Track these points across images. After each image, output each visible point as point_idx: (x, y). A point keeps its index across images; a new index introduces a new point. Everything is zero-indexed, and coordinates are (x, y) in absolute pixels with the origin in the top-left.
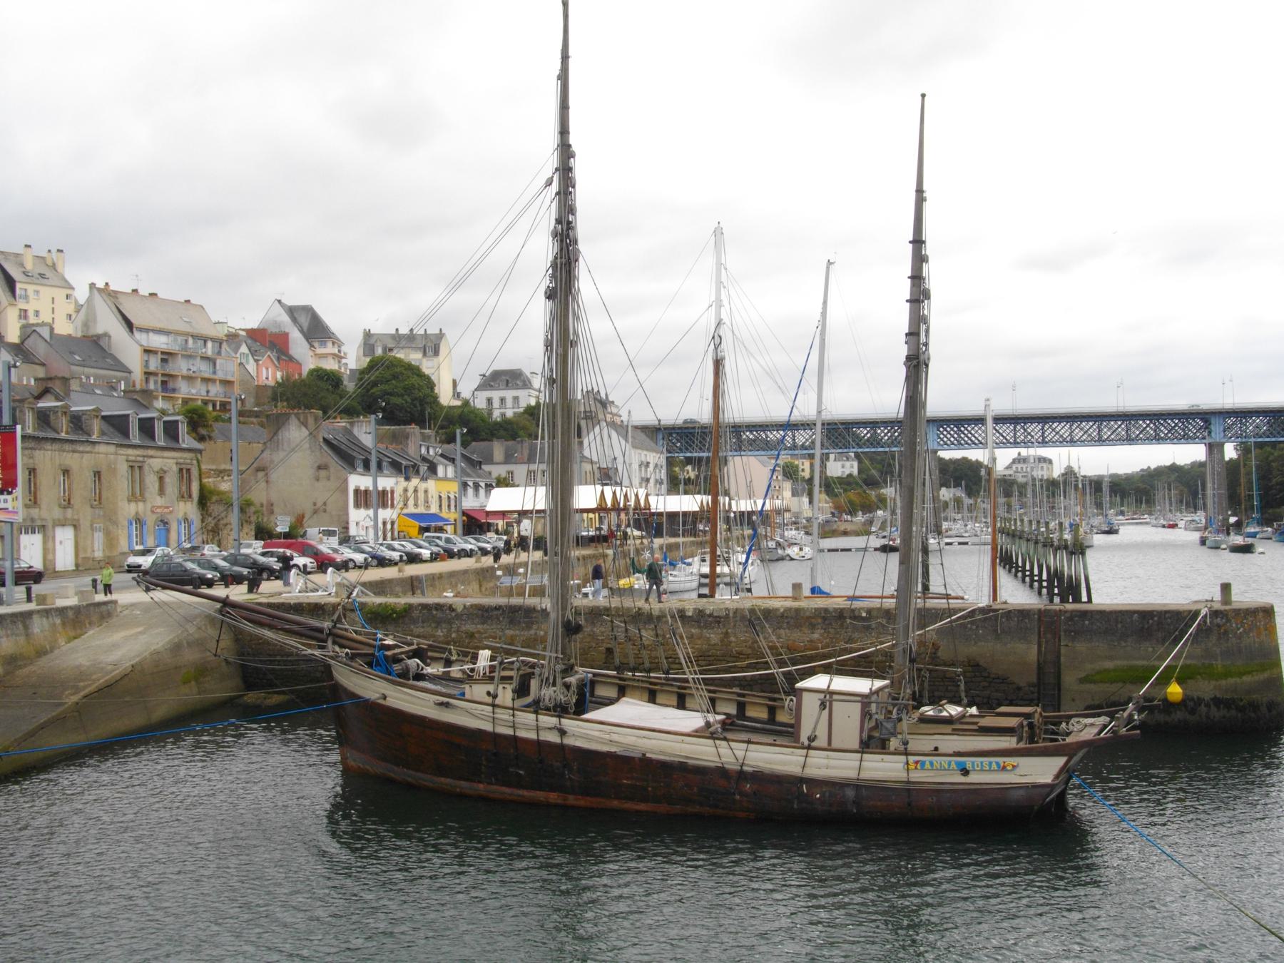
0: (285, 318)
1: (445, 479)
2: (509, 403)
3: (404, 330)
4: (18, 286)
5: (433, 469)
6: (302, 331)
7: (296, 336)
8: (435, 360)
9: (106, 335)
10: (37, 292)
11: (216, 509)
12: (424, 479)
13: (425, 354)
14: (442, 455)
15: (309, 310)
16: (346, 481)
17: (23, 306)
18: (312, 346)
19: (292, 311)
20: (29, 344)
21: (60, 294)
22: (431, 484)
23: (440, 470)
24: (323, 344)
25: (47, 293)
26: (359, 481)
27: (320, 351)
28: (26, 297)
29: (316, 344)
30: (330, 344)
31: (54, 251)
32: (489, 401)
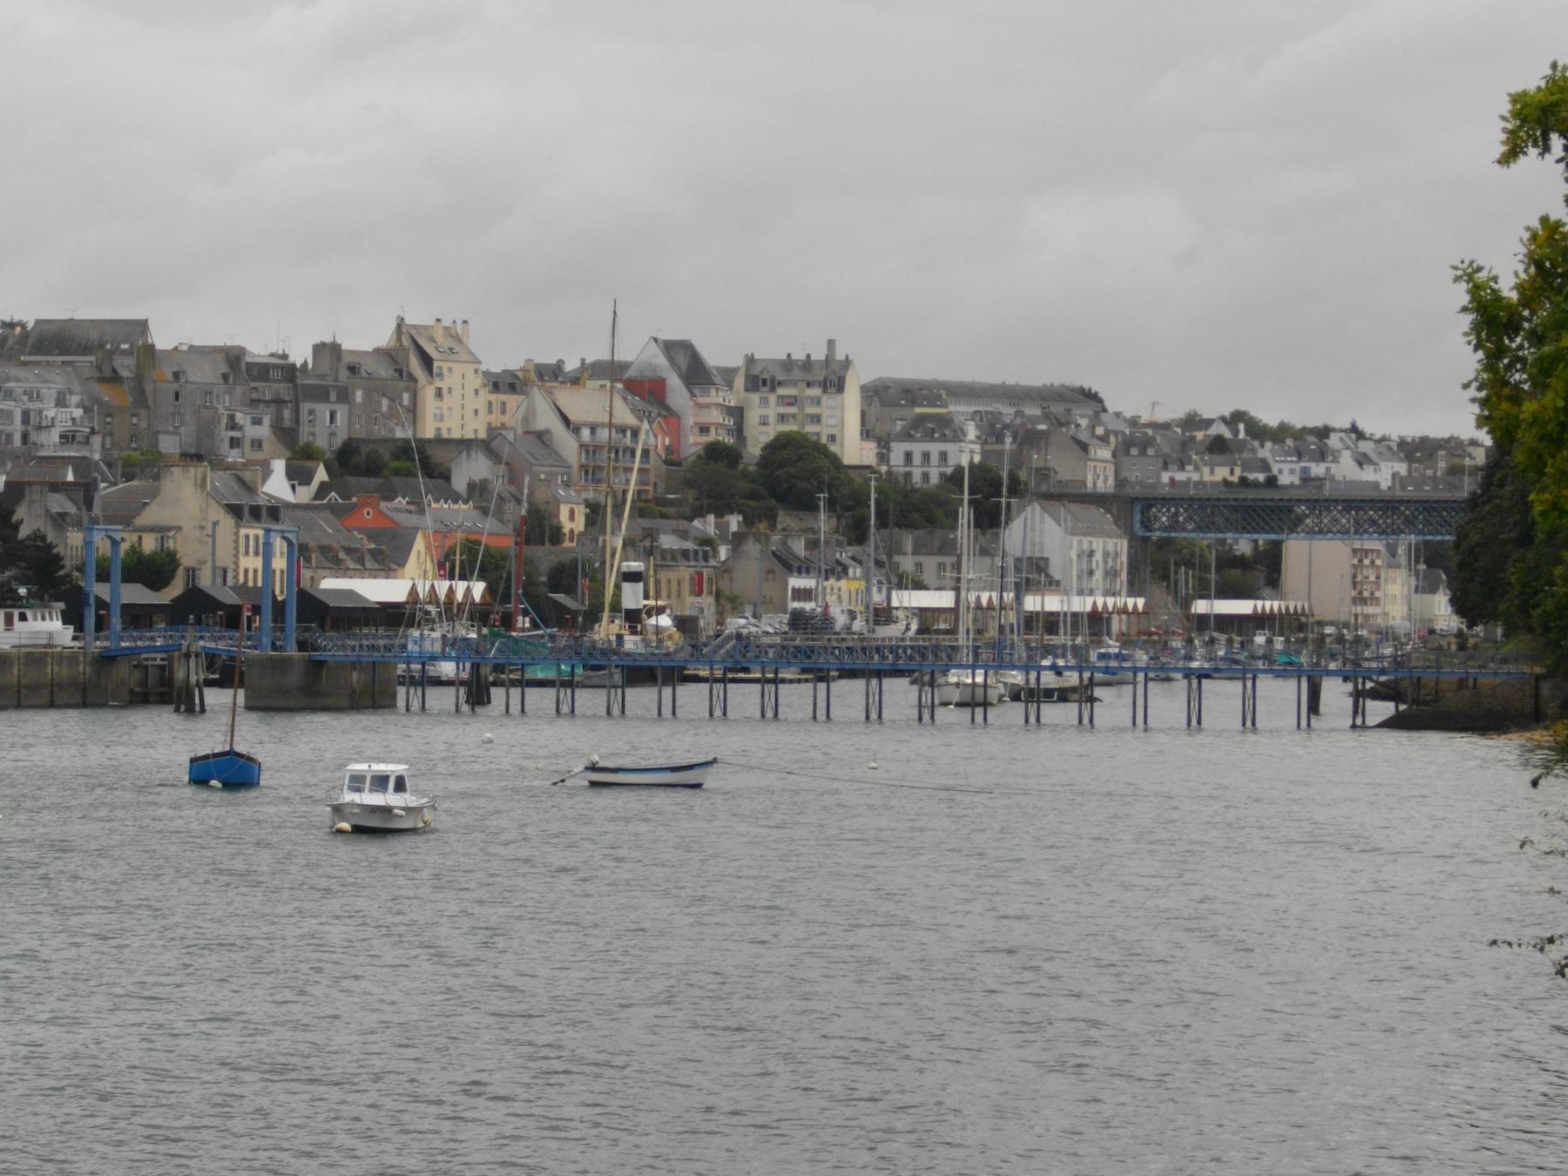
0: (662, 361)
1: (855, 579)
2: (934, 459)
3: (799, 356)
4: (436, 364)
5: (845, 569)
6: (680, 376)
7: (674, 382)
8: (839, 397)
9: (548, 431)
10: (450, 370)
11: (723, 601)
12: (839, 579)
13: (825, 391)
14: (853, 558)
15: (687, 347)
16: (786, 584)
17: (438, 384)
18: (693, 395)
19: (669, 347)
20: (495, 444)
21: (469, 369)
22: (843, 583)
23: (851, 571)
24: (706, 393)
25: (458, 369)
26: (795, 582)
27: (701, 400)
28: (440, 375)
29: (697, 392)
30: (713, 391)
31: (459, 323)
32: (908, 456)
